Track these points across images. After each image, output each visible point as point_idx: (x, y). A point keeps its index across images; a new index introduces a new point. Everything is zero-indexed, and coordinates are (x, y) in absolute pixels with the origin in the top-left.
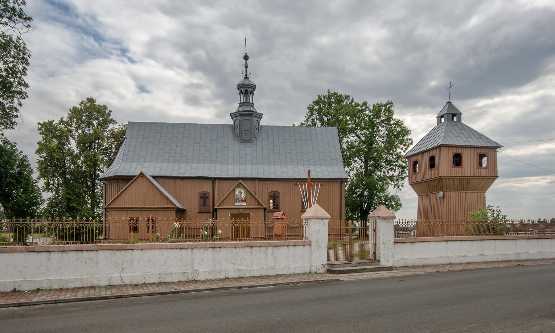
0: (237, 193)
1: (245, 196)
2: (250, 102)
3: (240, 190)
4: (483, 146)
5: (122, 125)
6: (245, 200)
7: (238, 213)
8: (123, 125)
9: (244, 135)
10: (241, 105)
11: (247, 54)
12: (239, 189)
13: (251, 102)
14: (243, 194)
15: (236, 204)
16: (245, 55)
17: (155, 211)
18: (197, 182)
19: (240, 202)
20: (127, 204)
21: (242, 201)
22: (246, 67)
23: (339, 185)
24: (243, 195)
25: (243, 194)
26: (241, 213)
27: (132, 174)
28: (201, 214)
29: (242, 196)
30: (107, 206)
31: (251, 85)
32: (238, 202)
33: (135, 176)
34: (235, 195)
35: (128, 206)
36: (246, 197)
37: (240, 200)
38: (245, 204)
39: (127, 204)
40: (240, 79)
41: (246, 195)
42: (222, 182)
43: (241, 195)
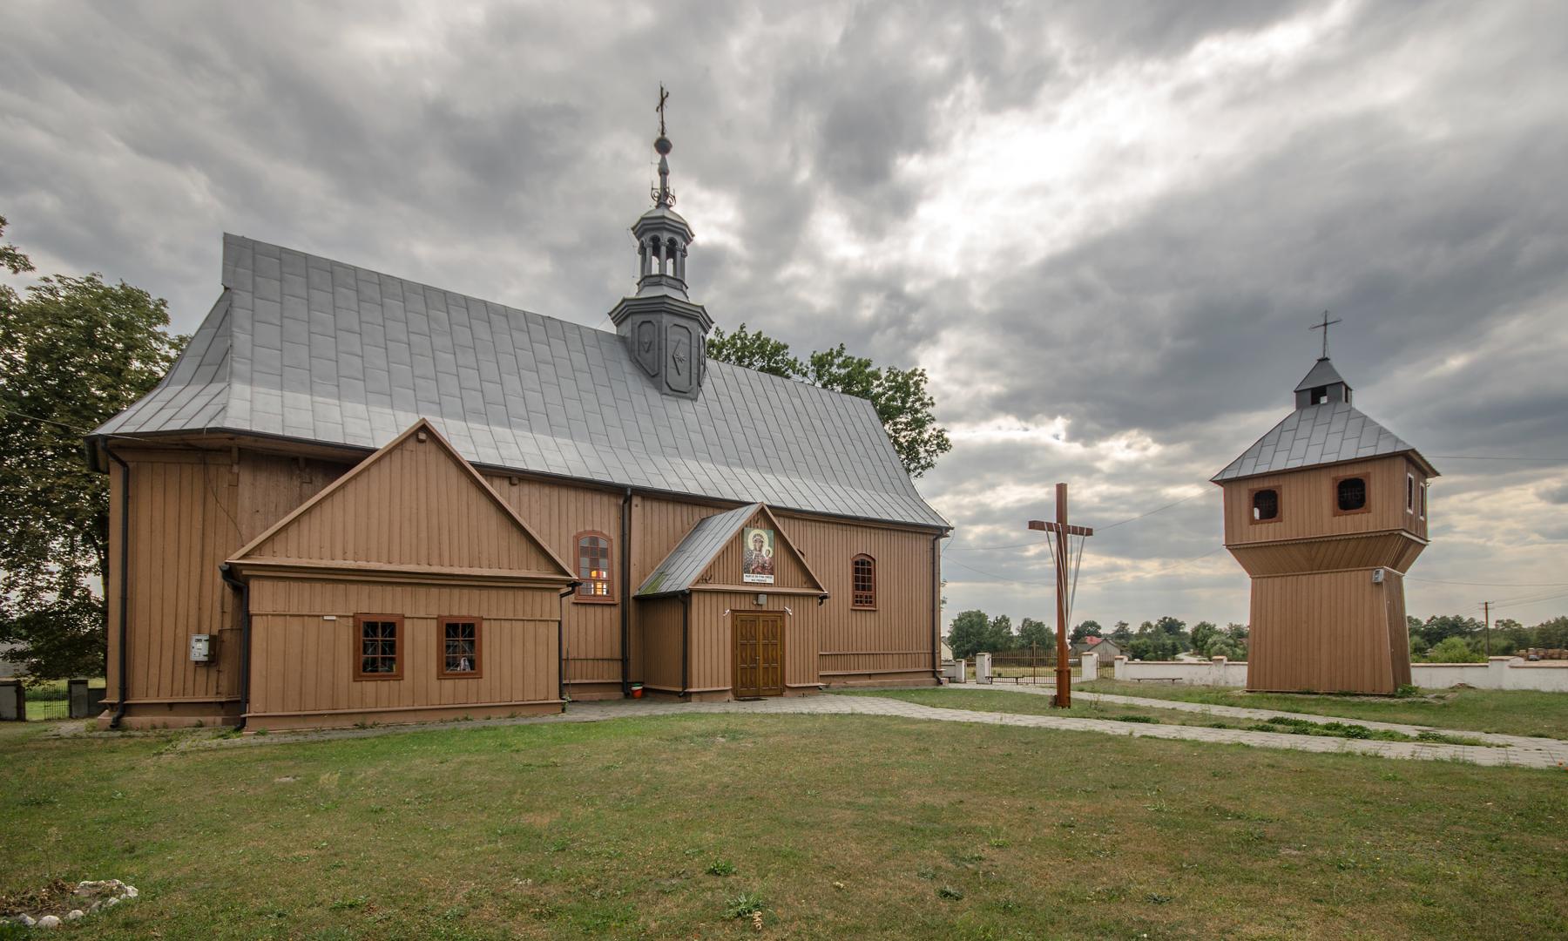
0: (750, 544)
1: (770, 556)
2: (668, 274)
3: (759, 535)
4: (617, 481)
5: (55, 280)
6: (772, 569)
7: (753, 608)
8: (60, 281)
9: (675, 371)
10: (647, 280)
11: (666, 136)
12: (757, 531)
13: (672, 275)
14: (766, 547)
15: (747, 578)
16: (659, 135)
17: (476, 592)
18: (569, 497)
19: (759, 573)
20: (345, 553)
21: (763, 569)
22: (663, 172)
23: (930, 545)
24: (767, 551)
25: (766, 547)
26: (759, 609)
27: (370, 445)
28: (582, 609)
29: (764, 553)
30: (239, 559)
31: (667, 221)
32: (753, 572)
33: (373, 451)
34: (745, 549)
35: (350, 564)
36: (773, 556)
37: (758, 567)
38: (770, 580)
39: (345, 553)
40: (649, 206)
41: (774, 551)
42: (656, 508)
43: (760, 550)
